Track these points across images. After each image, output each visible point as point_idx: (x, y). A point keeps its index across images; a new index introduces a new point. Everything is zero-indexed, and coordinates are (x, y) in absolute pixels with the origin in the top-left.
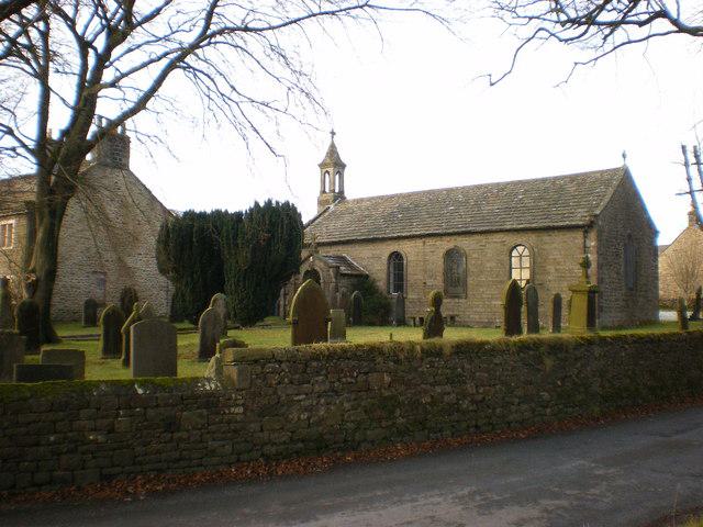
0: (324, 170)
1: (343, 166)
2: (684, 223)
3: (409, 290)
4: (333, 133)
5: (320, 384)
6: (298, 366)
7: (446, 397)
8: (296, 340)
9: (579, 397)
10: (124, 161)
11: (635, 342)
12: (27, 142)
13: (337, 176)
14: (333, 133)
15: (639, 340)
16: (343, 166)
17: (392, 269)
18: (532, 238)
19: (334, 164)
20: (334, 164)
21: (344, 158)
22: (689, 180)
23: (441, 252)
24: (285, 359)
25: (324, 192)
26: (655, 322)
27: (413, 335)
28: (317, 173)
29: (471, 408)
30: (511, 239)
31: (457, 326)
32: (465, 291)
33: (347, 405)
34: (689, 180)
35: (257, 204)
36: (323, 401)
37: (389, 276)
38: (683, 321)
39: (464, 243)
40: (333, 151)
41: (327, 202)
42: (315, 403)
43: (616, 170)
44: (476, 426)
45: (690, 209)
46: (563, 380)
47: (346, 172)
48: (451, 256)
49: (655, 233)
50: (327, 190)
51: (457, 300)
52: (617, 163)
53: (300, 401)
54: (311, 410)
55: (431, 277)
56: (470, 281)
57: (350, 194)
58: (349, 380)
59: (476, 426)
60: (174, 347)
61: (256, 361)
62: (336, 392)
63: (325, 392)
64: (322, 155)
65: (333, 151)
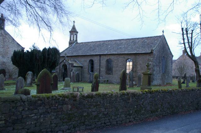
1: (77, 32)
2: (181, 53)
4: (74, 22)
5: (41, 110)
6: (34, 104)
7: (93, 113)
8: (38, 92)
9: (143, 112)
10: (2, 27)
11: (163, 92)
12: (9, 23)
13: (75, 36)
14: (74, 22)
15: (164, 92)
16: (77, 32)
17: (90, 65)
18: (133, 57)
19: (74, 31)
20: (74, 31)
22: (184, 39)
23: (88, 61)
24: (26, 100)
26: (169, 84)
27: (87, 88)
29: (102, 117)
30: (126, 57)
31: (109, 83)
32: (112, 72)
33: (53, 118)
34: (184, 39)
36: (42, 116)
37: (89, 66)
38: (180, 84)
39: (112, 57)
40: (74, 28)
42: (39, 117)
43: (160, 36)
44: (105, 123)
45: (183, 49)
46: (137, 106)
47: (78, 35)
49: (173, 56)
51: (110, 75)
52: (161, 34)
53: (32, 117)
54: (37, 120)
57: (79, 41)
58: (54, 108)
59: (105, 123)
61: (13, 102)
62: (48, 112)
63: (43, 112)
65: (74, 28)
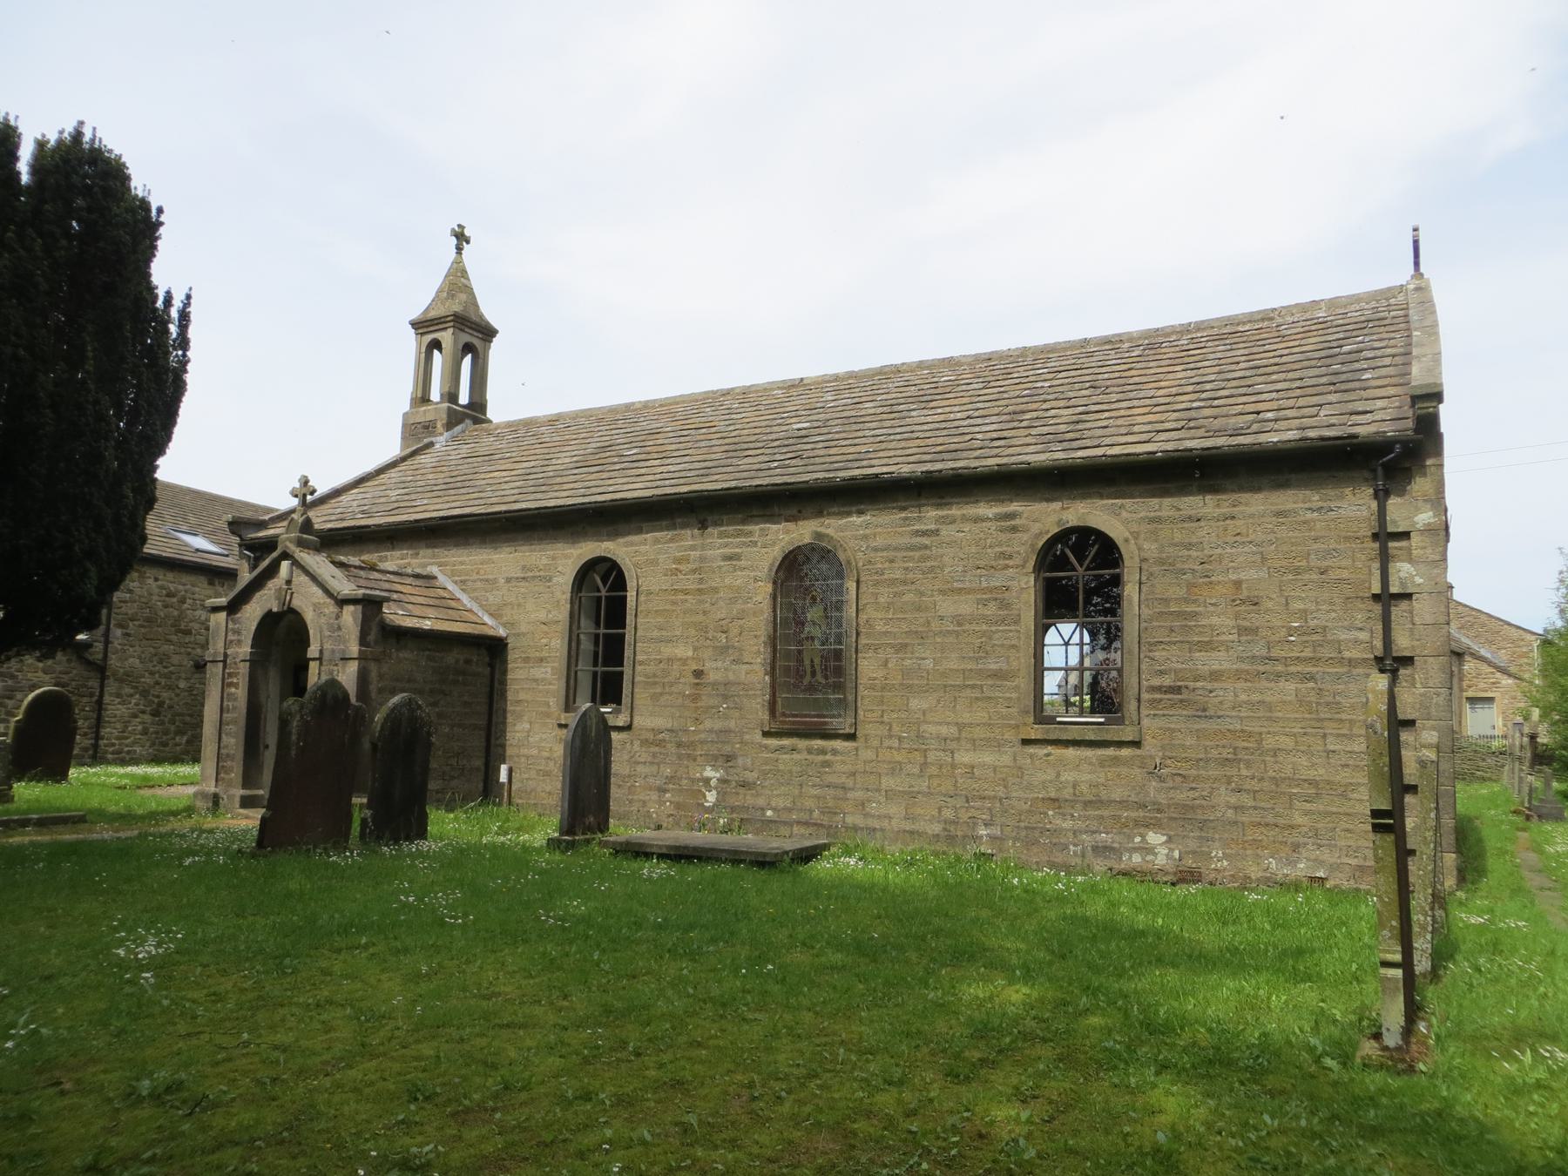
0: (429, 337)
1: (488, 333)
3: (642, 697)
4: (461, 237)
13: (467, 361)
14: (461, 237)
16: (488, 333)
19: (458, 329)
20: (458, 329)
21: (490, 312)
25: (422, 399)
28: (409, 345)
35: (78, 135)
40: (457, 282)
41: (429, 427)
48: (792, 566)
50: (435, 395)
55: (723, 650)
56: (868, 668)
60: (349, 804)
64: (421, 297)
65: (457, 282)
